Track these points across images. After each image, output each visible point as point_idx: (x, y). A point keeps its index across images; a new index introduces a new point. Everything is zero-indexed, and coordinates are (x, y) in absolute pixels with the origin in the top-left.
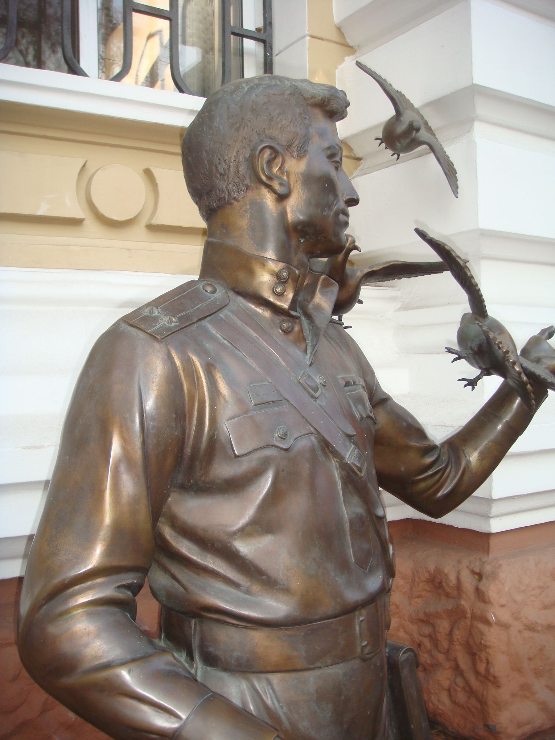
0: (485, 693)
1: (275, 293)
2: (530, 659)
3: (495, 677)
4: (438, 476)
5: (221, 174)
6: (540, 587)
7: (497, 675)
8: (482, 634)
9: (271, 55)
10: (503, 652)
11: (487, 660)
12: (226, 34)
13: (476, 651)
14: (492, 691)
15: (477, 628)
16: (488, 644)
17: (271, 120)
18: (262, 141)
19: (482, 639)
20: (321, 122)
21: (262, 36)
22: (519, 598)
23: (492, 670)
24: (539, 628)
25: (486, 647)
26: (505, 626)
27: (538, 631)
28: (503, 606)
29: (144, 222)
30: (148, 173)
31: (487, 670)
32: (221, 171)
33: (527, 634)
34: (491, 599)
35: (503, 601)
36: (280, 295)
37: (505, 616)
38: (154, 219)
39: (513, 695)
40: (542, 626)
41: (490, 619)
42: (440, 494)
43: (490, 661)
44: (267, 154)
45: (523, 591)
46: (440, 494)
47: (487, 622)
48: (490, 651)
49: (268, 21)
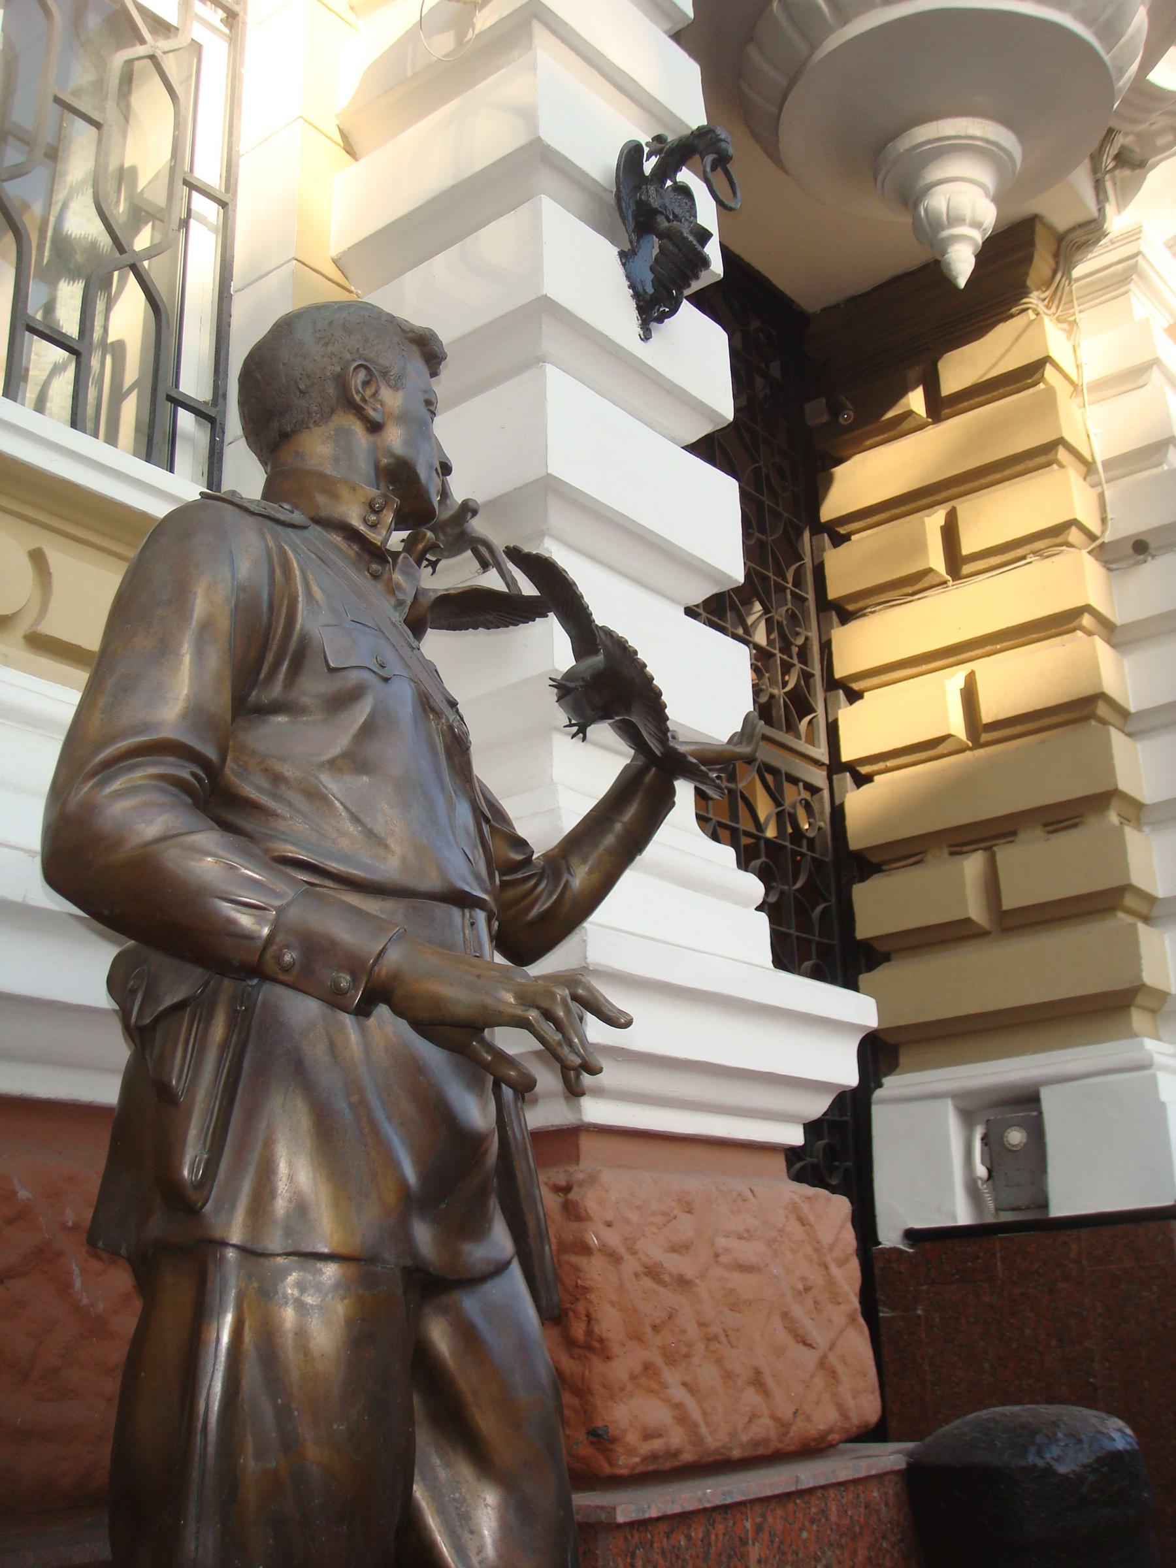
0: (587, 1373)
1: (365, 521)
2: (655, 1328)
3: (601, 1340)
4: (533, 882)
5: (301, 392)
6: (664, 1214)
7: (605, 1335)
8: (577, 1269)
9: (222, 441)
10: (613, 1304)
11: (588, 1315)
12: (158, 401)
13: (569, 1305)
14: (597, 1364)
15: (568, 1263)
16: (588, 1283)
17: (366, 341)
18: (354, 360)
19: (579, 1278)
20: (416, 366)
21: (212, 412)
22: (634, 1217)
23: (596, 1329)
24: (667, 1278)
25: (586, 1290)
26: (614, 1258)
27: (661, 1282)
28: (609, 1224)
29: (23, 626)
30: (38, 558)
31: (589, 1332)
32: (302, 387)
33: (648, 1283)
34: (590, 1211)
35: (609, 1216)
36: (373, 526)
37: (613, 1239)
38: (43, 623)
39: (633, 1377)
40: (670, 1274)
41: (591, 1243)
42: (534, 912)
43: (594, 1316)
44: (362, 375)
45: (639, 1208)
46: (534, 912)
47: (585, 1249)
48: (592, 1296)
49: (221, 392)
